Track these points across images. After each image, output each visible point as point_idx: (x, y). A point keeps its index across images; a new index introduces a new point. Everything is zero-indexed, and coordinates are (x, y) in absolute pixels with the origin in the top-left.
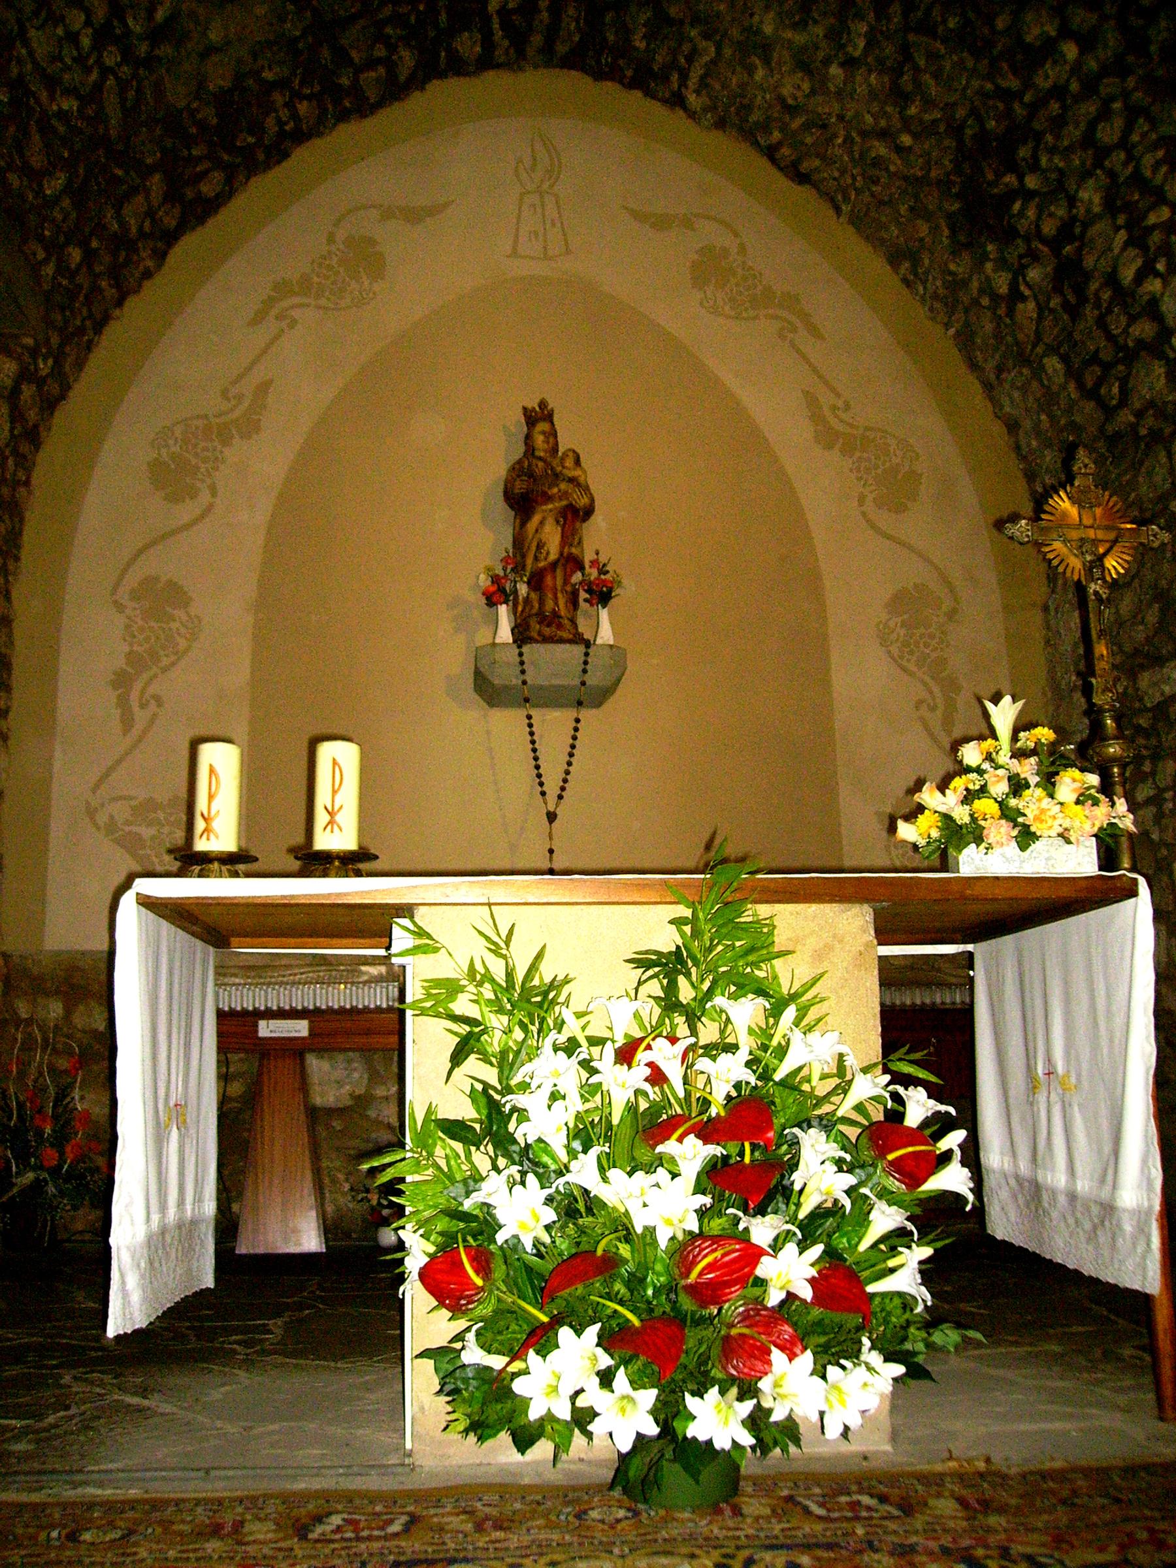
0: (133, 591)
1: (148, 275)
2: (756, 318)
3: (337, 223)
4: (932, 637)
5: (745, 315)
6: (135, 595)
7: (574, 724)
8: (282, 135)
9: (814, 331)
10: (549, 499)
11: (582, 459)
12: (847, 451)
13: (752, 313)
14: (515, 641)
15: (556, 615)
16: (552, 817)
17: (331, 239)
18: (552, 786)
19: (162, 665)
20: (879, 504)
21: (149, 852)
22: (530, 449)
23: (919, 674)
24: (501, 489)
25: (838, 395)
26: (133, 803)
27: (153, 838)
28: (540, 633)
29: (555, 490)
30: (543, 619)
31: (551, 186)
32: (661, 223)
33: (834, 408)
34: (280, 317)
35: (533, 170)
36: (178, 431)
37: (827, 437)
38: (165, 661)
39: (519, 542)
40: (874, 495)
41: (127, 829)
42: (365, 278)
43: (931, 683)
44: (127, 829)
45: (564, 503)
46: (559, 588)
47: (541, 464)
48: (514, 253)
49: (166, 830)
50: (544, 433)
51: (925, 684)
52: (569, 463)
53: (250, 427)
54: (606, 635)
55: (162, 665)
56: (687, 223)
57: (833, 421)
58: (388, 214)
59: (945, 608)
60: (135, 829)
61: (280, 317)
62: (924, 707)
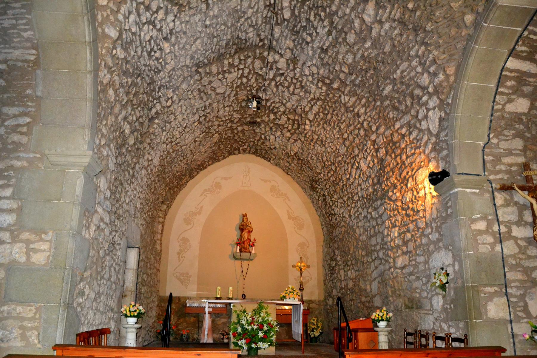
6: (181, 240)
9: (289, 200)
10: (246, 229)
12: (293, 220)
16: (244, 279)
18: (245, 274)
20: (298, 229)
22: (243, 221)
24: (238, 228)
30: (244, 248)
32: (266, 181)
37: (290, 218)
39: (241, 236)
53: (199, 213)
54: (253, 252)
56: (270, 181)
58: (222, 178)
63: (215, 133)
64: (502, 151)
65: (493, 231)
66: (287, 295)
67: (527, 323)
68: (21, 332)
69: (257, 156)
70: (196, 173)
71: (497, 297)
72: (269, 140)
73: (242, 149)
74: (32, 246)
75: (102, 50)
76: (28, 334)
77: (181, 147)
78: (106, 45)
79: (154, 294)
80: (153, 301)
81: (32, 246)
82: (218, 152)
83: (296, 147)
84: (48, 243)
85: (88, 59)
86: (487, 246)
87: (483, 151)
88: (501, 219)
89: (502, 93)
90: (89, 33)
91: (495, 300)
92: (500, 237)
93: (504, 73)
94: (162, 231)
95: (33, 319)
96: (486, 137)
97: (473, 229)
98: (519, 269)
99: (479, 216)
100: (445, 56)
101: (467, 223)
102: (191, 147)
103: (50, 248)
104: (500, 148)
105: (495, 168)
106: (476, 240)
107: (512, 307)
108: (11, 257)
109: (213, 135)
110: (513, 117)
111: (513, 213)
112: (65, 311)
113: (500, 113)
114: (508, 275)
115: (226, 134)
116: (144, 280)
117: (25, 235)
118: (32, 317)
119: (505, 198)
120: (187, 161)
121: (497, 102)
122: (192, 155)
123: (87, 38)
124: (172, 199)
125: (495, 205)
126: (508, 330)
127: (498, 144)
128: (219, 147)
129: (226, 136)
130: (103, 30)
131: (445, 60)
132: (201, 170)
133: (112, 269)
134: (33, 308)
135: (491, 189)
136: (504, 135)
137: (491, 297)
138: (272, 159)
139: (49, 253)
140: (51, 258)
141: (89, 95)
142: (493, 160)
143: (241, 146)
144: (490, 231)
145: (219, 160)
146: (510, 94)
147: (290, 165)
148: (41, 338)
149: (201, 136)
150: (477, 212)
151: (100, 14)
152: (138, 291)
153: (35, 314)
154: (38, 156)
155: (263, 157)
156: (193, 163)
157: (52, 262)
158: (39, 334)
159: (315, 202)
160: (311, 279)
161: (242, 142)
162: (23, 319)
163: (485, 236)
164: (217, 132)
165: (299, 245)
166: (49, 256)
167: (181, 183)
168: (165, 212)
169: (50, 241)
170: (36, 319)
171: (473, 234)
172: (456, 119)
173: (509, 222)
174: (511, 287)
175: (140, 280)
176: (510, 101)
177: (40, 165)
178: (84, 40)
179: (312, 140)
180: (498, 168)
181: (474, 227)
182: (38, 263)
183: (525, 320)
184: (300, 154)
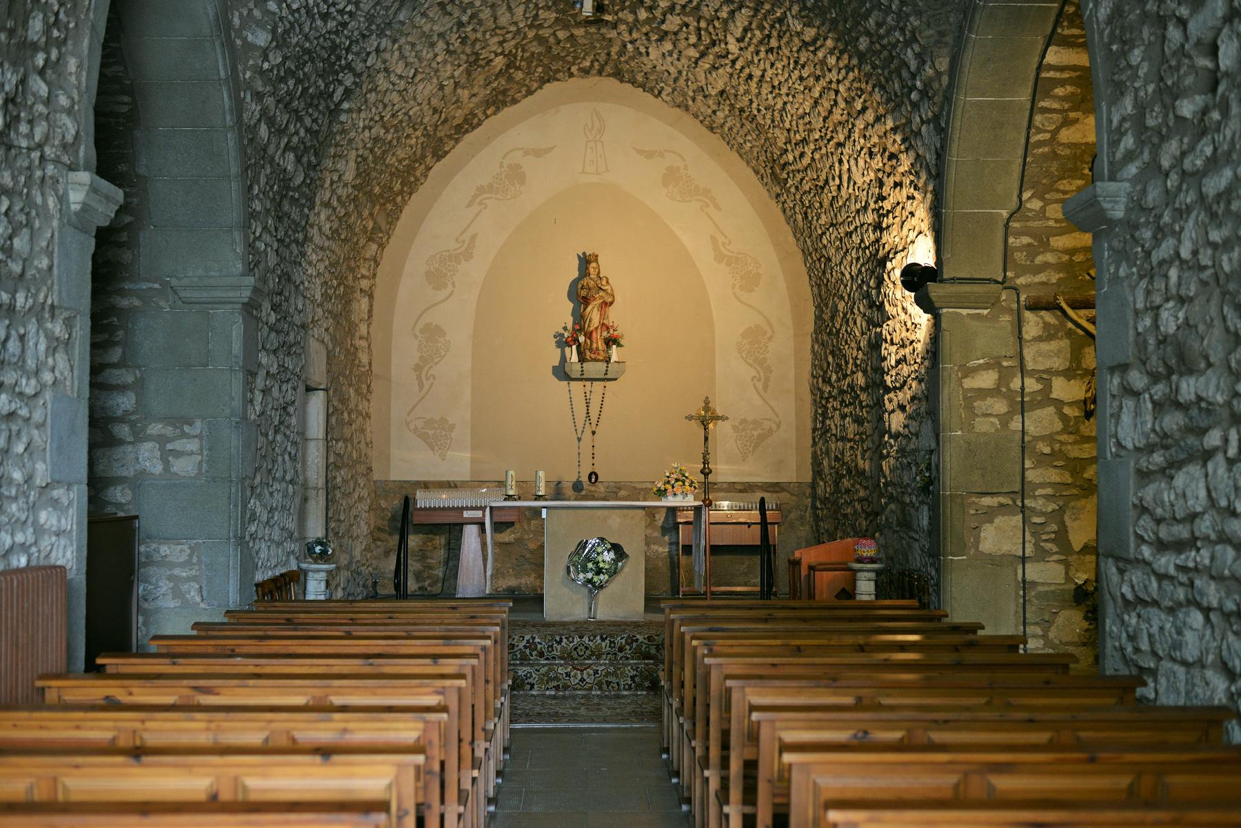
0: (421, 330)
3: (504, 157)
6: (422, 331)
9: (717, 207)
12: (728, 264)
13: (688, 199)
15: (597, 349)
16: (594, 433)
18: (594, 421)
25: (726, 237)
30: (591, 350)
32: (650, 155)
33: (724, 244)
34: (480, 203)
37: (719, 258)
38: (436, 360)
48: (583, 172)
51: (755, 368)
52: (604, 282)
53: (468, 255)
57: (723, 250)
58: (527, 153)
59: (768, 335)
61: (480, 203)
64: (1051, 223)
65: (1009, 389)
66: (669, 487)
67: (1059, 561)
68: (172, 584)
69: (622, 81)
71: (1003, 516)
74: (169, 446)
75: (244, 74)
76: (185, 587)
78: (251, 62)
79: (361, 481)
80: (360, 499)
81: (169, 446)
83: (719, 81)
84: (197, 440)
85: (227, 107)
86: (992, 419)
87: (1007, 226)
88: (1030, 366)
89: (1045, 110)
90: (225, 65)
91: (998, 520)
92: (1023, 402)
93: (1044, 75)
94: (370, 311)
95: (187, 564)
96: (1015, 198)
97: (966, 387)
98: (1055, 464)
99: (981, 361)
100: (931, 32)
101: (953, 376)
103: (202, 450)
104: (1048, 219)
105: (1032, 261)
106: (970, 408)
107: (1033, 534)
108: (138, 467)
110: (1079, 151)
111: (1058, 353)
112: (236, 549)
113: (1046, 149)
114: (1031, 475)
116: (339, 455)
117: (155, 429)
118: (186, 561)
119: (1045, 323)
120: (425, 129)
121: (1038, 128)
122: (436, 116)
123: (222, 74)
125: (1020, 338)
126: (1016, 574)
127: (1043, 210)
130: (245, 40)
131: (932, 40)
133: (287, 457)
134: (185, 547)
135: (1015, 306)
136: (1058, 191)
137: (989, 515)
139: (200, 457)
140: (204, 465)
141: (234, 169)
142: (1029, 245)
144: (1004, 390)
145: (515, 101)
146: (1067, 111)
148: (205, 593)
150: (979, 354)
151: (237, 14)
152: (329, 485)
153: (190, 556)
154: (157, 286)
157: (207, 471)
158: (201, 587)
160: (779, 426)
162: (173, 565)
163: (989, 401)
165: (744, 335)
166: (200, 462)
169: (199, 437)
170: (194, 564)
171: (965, 398)
172: (948, 166)
173: (1047, 371)
174: (1035, 497)
175: (331, 460)
176: (1067, 123)
177: (162, 303)
178: (216, 77)
180: (1039, 259)
181: (968, 383)
182: (183, 474)
183: (1055, 557)
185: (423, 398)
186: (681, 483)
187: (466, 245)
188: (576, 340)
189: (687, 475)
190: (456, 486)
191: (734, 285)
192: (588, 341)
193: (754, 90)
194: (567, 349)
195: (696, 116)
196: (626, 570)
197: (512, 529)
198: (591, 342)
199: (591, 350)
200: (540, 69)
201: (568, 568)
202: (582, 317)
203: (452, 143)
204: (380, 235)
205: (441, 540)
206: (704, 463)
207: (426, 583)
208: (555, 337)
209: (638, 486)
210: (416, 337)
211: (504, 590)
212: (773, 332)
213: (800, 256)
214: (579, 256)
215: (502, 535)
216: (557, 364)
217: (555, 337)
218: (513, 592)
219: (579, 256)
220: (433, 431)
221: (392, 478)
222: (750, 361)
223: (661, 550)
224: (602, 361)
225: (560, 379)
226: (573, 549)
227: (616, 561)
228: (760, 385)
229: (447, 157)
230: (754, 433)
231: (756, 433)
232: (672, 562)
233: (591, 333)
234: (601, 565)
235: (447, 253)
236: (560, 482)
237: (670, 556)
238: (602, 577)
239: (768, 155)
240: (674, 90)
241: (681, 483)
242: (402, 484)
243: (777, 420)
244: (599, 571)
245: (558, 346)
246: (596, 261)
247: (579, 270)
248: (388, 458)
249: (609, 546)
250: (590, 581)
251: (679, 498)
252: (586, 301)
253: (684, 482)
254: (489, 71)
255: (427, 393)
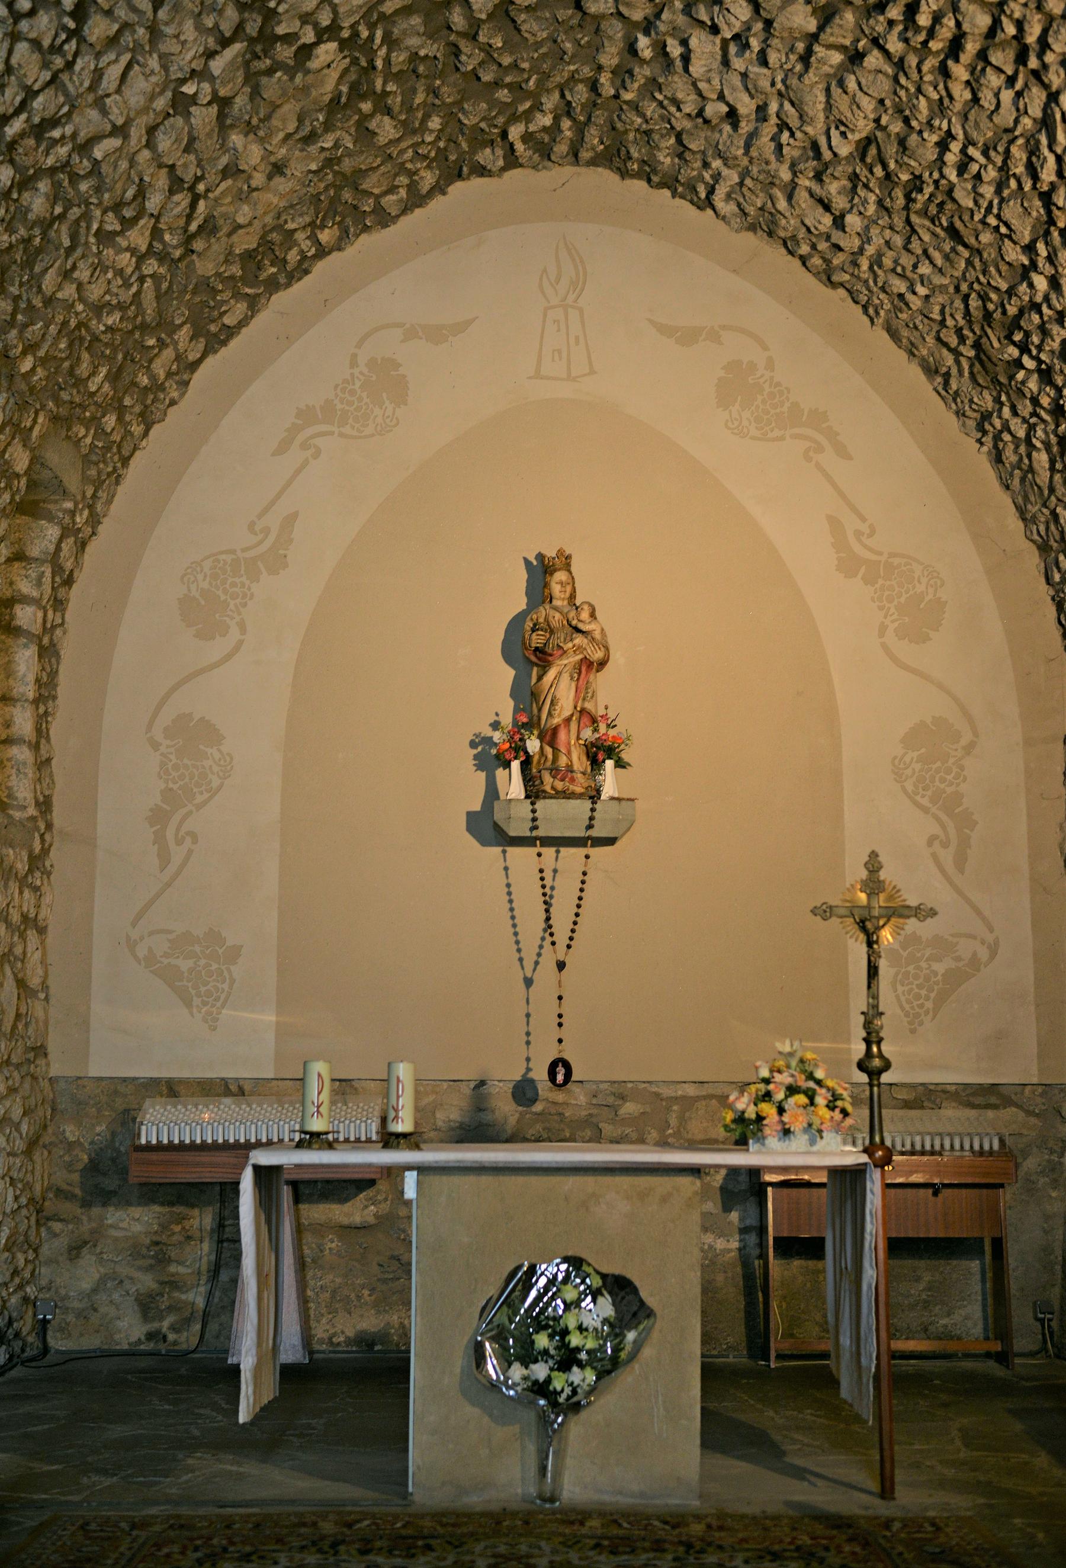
0: (166, 729)
1: (173, 403)
2: (782, 438)
3: (359, 345)
4: (948, 771)
5: (770, 435)
7: (577, 902)
8: (304, 258)
9: (842, 452)
11: (597, 614)
12: (868, 581)
13: (777, 433)
14: (527, 797)
15: (570, 769)
16: (561, 966)
17: (354, 364)
19: (196, 802)
21: (185, 983)
23: (934, 810)
25: (863, 519)
26: (171, 937)
27: (191, 970)
28: (553, 788)
29: (570, 645)
30: (554, 771)
31: (575, 301)
32: (688, 337)
33: (858, 534)
34: (304, 446)
35: (558, 280)
36: (207, 565)
37: (849, 565)
38: (199, 799)
40: (896, 624)
41: (166, 961)
42: (387, 403)
43: (944, 818)
44: (166, 961)
45: (580, 657)
46: (573, 742)
47: (558, 615)
48: (538, 375)
49: (203, 962)
50: (561, 583)
51: (937, 819)
52: (585, 615)
53: (277, 562)
55: (196, 802)
57: (857, 548)
58: (411, 334)
59: (964, 742)
60: (174, 962)
61: (304, 446)
62: (936, 843)
63: (308, 36)
66: (768, 1110)
69: (624, 174)
70: (241, 308)
72: (686, 59)
73: (527, 138)
77: (84, 148)
82: (363, 161)
102: (164, 142)
109: (306, 52)
115: (390, 41)
124: (98, 484)
128: (365, 134)
129: (399, 58)
132: (273, 286)
138: (721, 191)
143: (514, 118)
145: (384, 219)
147: (839, 222)
149: (217, 66)
155: (670, 183)
156: (198, 245)
159: (1010, 456)
160: (994, 952)
161: (517, 88)
164: (324, 34)
167: (145, 381)
168: (57, 569)
179: (955, 47)
184: (891, 150)
185: (168, 885)
186: (802, 1099)
187: (272, 538)
188: (519, 748)
189: (819, 1074)
190: (241, 1092)
191: (882, 630)
192: (549, 750)
193: (962, 94)
194: (500, 773)
195: (789, 245)
196: (647, 1352)
197: (370, 1192)
198: (556, 750)
199: (554, 771)
200: (435, 123)
201: (479, 1349)
202: (534, 695)
203: (241, 307)
204: (69, 505)
205: (202, 1219)
206: (868, 1042)
207: (166, 1324)
208: (473, 744)
209: (666, 1092)
210: (155, 745)
211: (349, 1341)
212: (976, 734)
213: (1033, 560)
214: (526, 561)
215: (347, 1207)
216: (477, 807)
217: (473, 744)
218: (371, 1345)
219: (526, 561)
220: (190, 963)
221: (93, 1072)
222: (925, 802)
223: (720, 1244)
224: (580, 796)
225: (484, 843)
226: (493, 1291)
227: (616, 1327)
228: (947, 857)
229: (234, 343)
230: (936, 966)
231: (940, 968)
232: (748, 1277)
233: (555, 731)
234: (575, 1340)
235: (229, 558)
236: (482, 1083)
237: (745, 1260)
238: (576, 1375)
239: (974, 303)
240: (745, 174)
241: (802, 1099)
242: (116, 1086)
243: (990, 938)
244: (568, 1359)
245: (479, 767)
246: (567, 567)
247: (529, 593)
248: (85, 1025)
249: (594, 1281)
250: (541, 1388)
251: (800, 1141)
252: (542, 658)
253: (811, 1096)
254: (305, 90)
255: (178, 873)
